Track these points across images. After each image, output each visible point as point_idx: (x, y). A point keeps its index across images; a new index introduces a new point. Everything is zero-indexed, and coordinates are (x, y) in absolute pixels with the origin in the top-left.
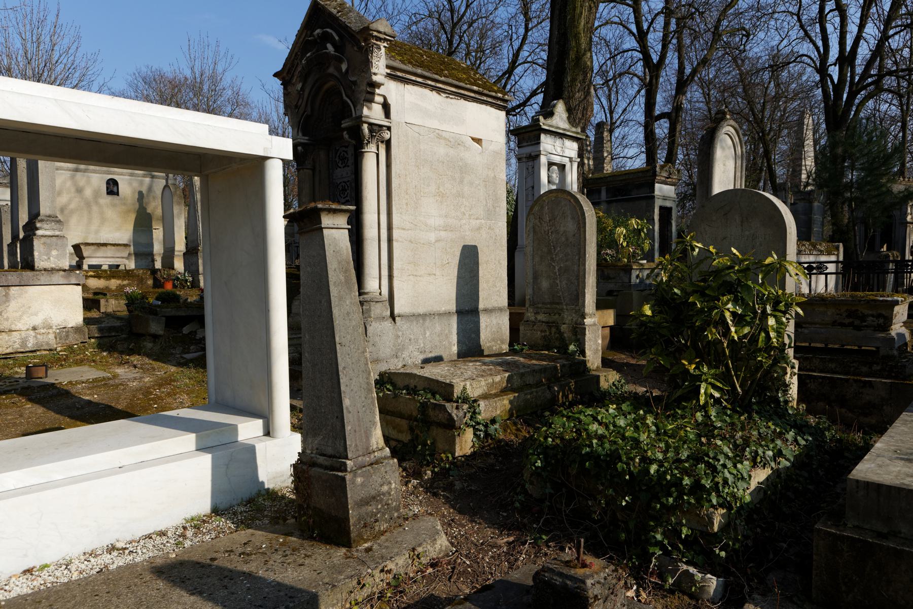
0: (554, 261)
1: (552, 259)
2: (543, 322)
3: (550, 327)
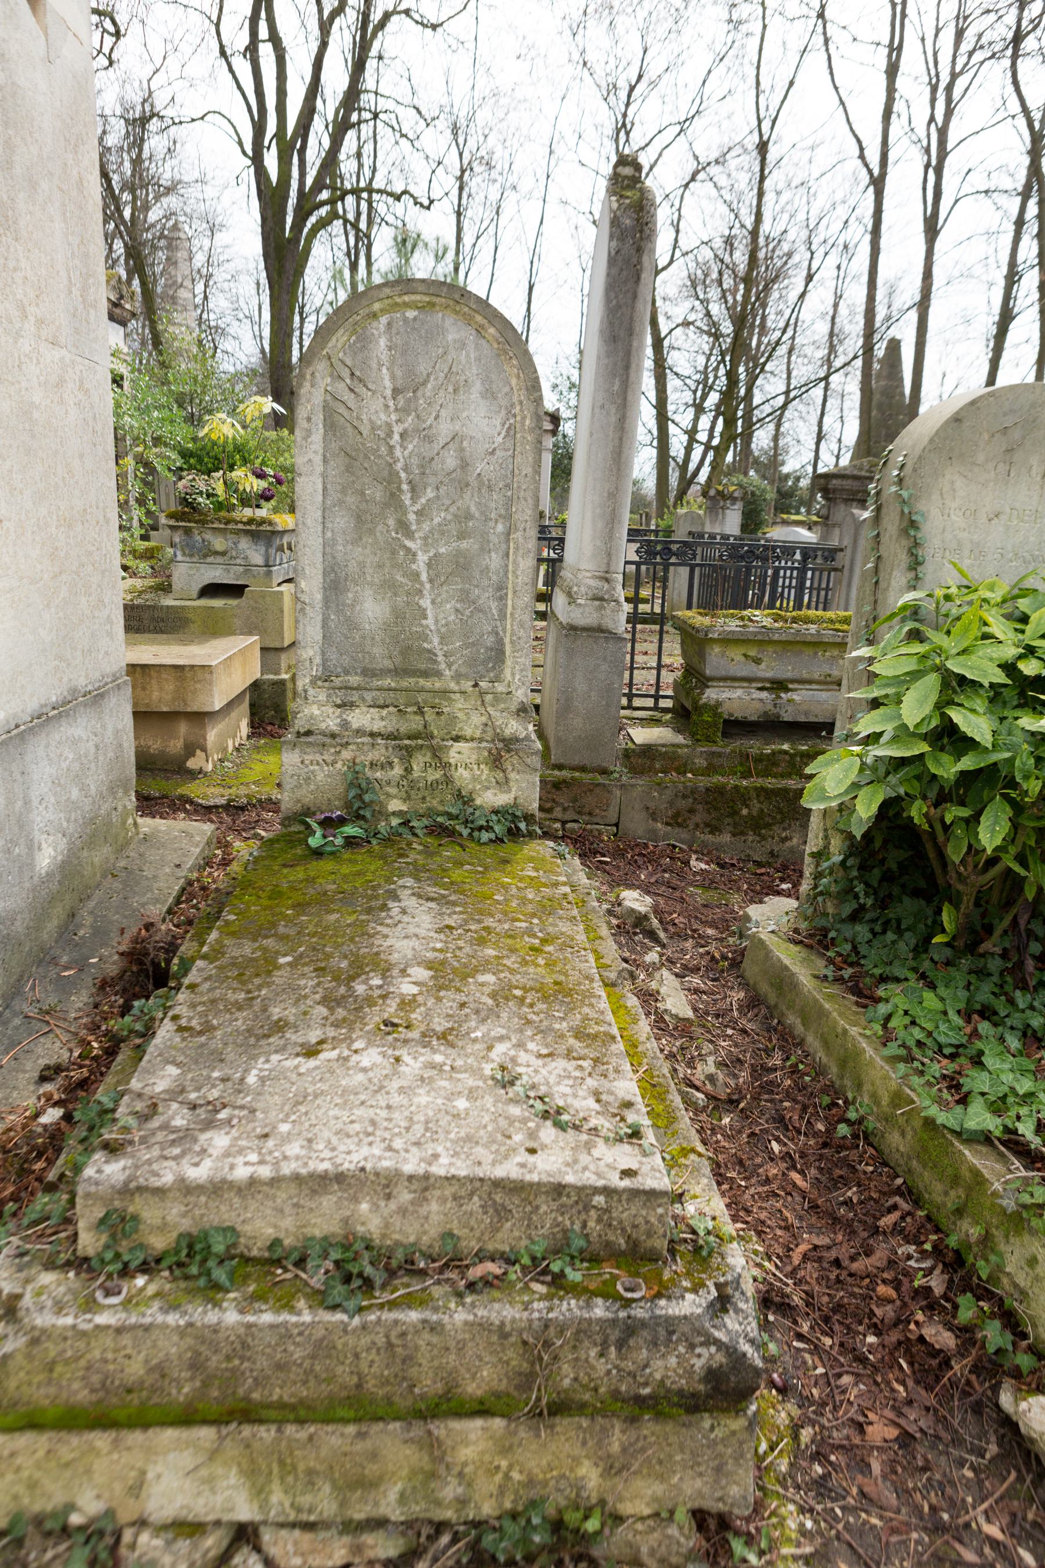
0: (410, 535)
1: (403, 526)
2: (372, 735)
3: (408, 753)
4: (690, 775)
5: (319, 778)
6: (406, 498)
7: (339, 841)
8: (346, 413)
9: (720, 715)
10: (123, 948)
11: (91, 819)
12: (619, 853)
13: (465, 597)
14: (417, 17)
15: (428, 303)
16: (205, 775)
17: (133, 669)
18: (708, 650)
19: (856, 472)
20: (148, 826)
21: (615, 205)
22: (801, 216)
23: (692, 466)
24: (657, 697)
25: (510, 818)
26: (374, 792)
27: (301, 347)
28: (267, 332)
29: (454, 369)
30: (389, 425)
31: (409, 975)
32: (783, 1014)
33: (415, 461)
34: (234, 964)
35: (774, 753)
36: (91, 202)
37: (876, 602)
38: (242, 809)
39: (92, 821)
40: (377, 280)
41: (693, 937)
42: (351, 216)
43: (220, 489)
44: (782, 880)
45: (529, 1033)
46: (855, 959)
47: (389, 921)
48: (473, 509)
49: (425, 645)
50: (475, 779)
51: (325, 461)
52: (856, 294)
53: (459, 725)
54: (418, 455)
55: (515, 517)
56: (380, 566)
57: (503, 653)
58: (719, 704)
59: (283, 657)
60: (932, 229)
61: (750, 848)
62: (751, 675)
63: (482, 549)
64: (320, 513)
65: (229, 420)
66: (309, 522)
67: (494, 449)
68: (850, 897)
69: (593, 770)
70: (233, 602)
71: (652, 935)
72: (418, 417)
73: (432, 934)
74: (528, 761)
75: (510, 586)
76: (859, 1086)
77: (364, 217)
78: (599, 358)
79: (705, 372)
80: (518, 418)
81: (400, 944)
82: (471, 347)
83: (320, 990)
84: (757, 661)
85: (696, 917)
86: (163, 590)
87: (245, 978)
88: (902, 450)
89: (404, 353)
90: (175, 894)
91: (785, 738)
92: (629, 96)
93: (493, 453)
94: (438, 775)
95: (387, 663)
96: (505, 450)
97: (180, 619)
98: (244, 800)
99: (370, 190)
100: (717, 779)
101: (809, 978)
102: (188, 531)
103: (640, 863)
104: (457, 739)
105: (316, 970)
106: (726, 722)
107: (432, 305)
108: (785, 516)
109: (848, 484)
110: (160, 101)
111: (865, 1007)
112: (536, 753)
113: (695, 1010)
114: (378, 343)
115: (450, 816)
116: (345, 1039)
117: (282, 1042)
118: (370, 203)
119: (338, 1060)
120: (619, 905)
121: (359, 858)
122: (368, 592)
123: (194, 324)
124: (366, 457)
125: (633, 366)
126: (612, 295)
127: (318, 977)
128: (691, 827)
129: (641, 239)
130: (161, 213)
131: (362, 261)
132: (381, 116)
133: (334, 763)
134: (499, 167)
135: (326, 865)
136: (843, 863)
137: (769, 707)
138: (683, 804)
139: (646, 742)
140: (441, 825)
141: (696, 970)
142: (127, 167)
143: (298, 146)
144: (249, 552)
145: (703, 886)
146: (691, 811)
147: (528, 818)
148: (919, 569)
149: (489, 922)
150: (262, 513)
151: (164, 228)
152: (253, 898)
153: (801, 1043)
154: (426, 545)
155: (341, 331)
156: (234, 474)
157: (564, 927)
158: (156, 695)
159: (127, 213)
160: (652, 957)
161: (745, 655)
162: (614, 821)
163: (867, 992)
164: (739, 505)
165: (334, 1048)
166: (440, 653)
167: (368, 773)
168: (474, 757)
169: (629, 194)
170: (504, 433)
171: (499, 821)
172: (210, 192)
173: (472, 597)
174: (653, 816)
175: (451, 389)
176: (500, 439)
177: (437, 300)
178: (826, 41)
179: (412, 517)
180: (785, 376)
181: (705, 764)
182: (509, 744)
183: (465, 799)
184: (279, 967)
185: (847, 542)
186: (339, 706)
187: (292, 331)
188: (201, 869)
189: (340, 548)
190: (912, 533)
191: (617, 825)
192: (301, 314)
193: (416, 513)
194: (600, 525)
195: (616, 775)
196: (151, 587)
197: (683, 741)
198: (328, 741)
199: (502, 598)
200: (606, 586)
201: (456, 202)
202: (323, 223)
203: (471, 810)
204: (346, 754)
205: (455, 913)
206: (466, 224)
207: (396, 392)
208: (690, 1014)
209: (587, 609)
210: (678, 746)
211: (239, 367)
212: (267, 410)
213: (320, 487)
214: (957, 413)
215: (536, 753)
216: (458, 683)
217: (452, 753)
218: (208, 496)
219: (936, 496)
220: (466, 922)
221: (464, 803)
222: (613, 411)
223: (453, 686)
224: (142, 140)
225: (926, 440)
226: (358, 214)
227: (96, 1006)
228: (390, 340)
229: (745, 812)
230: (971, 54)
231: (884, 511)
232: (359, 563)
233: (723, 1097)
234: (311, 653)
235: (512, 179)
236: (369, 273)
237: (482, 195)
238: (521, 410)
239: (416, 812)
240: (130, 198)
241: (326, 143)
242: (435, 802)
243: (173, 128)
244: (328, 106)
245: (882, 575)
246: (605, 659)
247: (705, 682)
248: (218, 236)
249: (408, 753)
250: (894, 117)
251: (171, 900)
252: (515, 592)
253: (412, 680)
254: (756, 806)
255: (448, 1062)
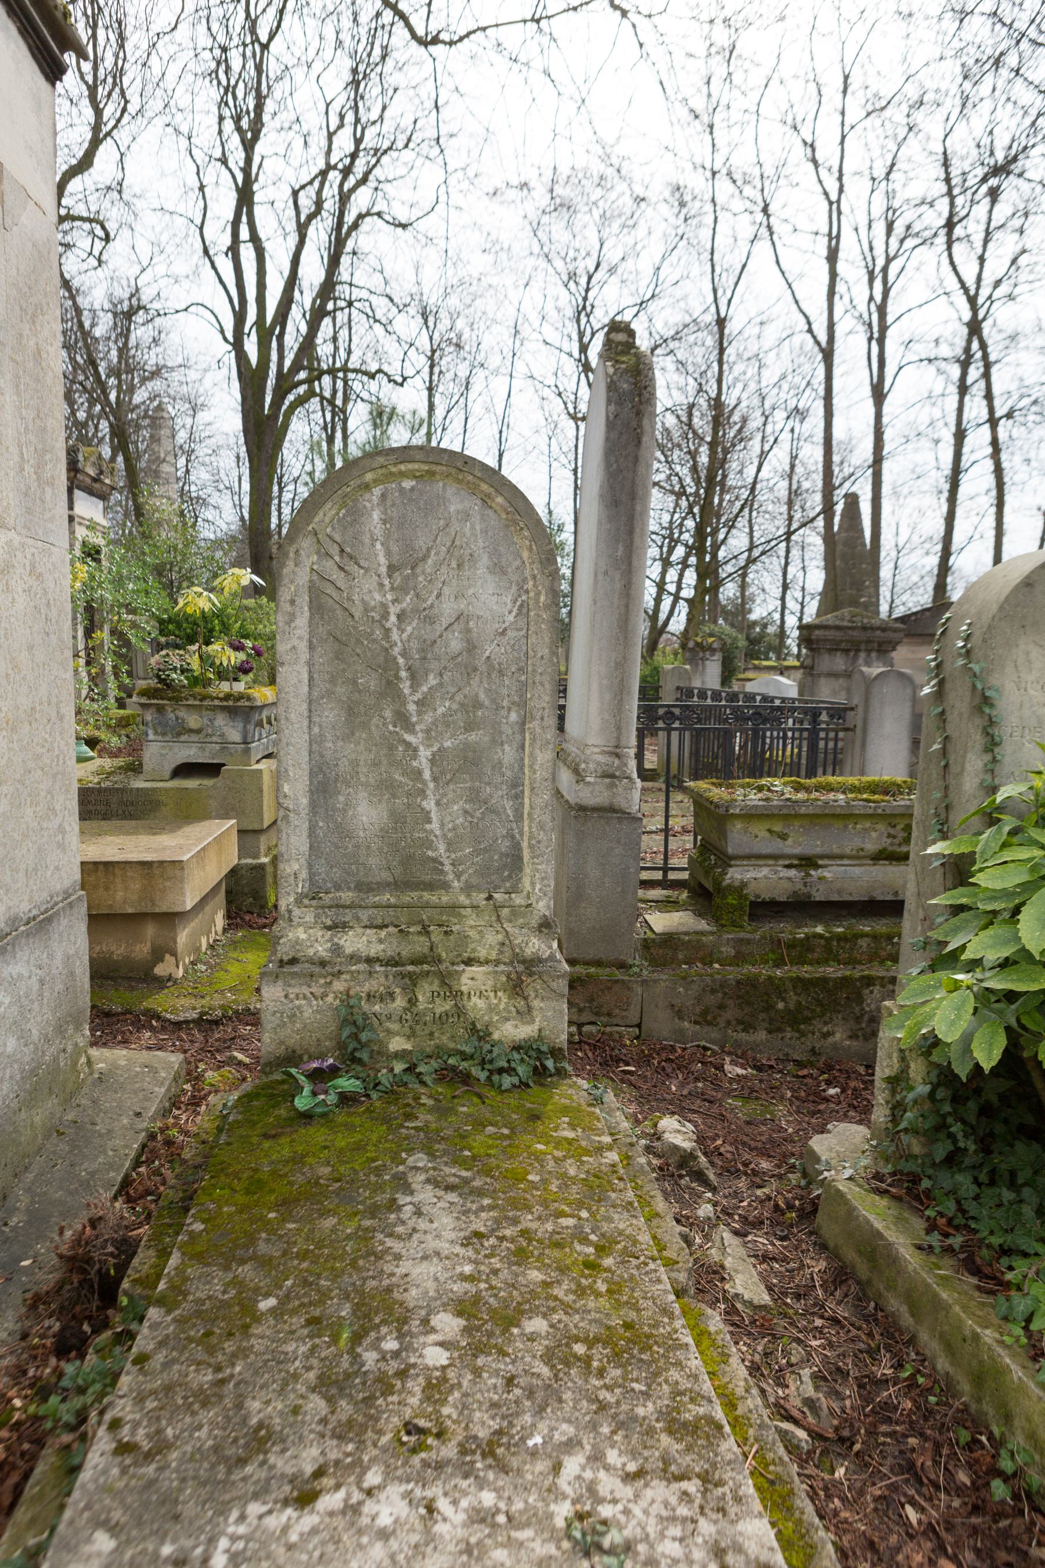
0: (410, 728)
1: (402, 719)
2: (369, 960)
4: (717, 966)
5: (306, 1015)
6: (405, 687)
7: (332, 1098)
8: (334, 594)
9: (744, 897)
10: (64, 1249)
11: (32, 1071)
12: (644, 1060)
13: (474, 796)
14: (387, 217)
15: (427, 471)
16: (175, 982)
17: (91, 869)
18: (729, 826)
19: (837, 623)
20: (105, 1061)
21: (611, 370)
22: (753, 386)
23: (662, 616)
24: (665, 869)
25: (534, 1054)
26: (372, 1029)
27: (280, 514)
28: (246, 501)
29: (457, 543)
30: (384, 606)
31: (433, 1330)
32: (880, 1295)
33: (414, 645)
34: (198, 1314)
35: (807, 938)
36: (50, 374)
37: (946, 788)
38: (217, 1023)
39: (33, 1072)
40: (354, 451)
41: (746, 1174)
42: (327, 394)
43: (195, 663)
44: (829, 1083)
45: (605, 1430)
46: (964, 1222)
47: (400, 1229)
48: (482, 696)
49: (430, 853)
50: (491, 1009)
51: (311, 647)
52: (812, 454)
53: (472, 946)
54: (418, 638)
55: (531, 704)
56: (376, 764)
57: (520, 858)
58: (744, 885)
59: (263, 839)
60: (879, 394)
61: (789, 1046)
62: (777, 852)
63: (494, 741)
64: (305, 706)
65: (205, 593)
66: (293, 717)
67: (505, 629)
68: (942, 1135)
69: (610, 964)
70: (208, 782)
71: (699, 1176)
72: (417, 596)
73: (458, 1249)
74: (554, 985)
75: (527, 782)
76: (1008, 1418)
77: (340, 395)
78: (600, 523)
79: (670, 528)
80: (532, 594)
81: (418, 1270)
82: (476, 518)
83: (315, 1362)
84: (783, 837)
85: (744, 1144)
86: (134, 770)
87: (214, 1340)
88: (964, 617)
89: (401, 526)
90: (133, 1154)
91: (818, 919)
92: (588, 283)
93: (503, 633)
94: (448, 1006)
95: (385, 876)
96: (518, 630)
97: (151, 802)
98: (219, 1013)
99: (345, 369)
100: (748, 969)
101: (912, 1249)
102: (160, 709)
103: (669, 1070)
104: (469, 962)
105: (309, 1322)
106: (753, 904)
107: (432, 473)
108: (756, 662)
109: (830, 634)
110: (146, 296)
111: (991, 1293)
112: (563, 976)
113: (770, 1289)
114: (371, 516)
115: (465, 1057)
116: (353, 1465)
117: (263, 1474)
118: (345, 381)
119: (343, 1512)
120: (659, 1139)
121: (357, 1121)
122: (362, 794)
123: (175, 496)
124: (358, 641)
125: (637, 530)
126: (613, 459)
127: (311, 1336)
128: (722, 1025)
129: (641, 402)
130: (146, 395)
131: (339, 435)
132: (356, 304)
133: (324, 996)
134: (467, 348)
135: (318, 1134)
136: (932, 1095)
137: (799, 886)
138: (712, 1000)
139: (667, 930)
140: (453, 1069)
141: (758, 1224)
142: (114, 353)
143: (277, 332)
144: (225, 729)
145: (741, 1097)
146: (722, 1007)
147: (555, 1053)
148: (996, 750)
149: (528, 1221)
150: (240, 687)
151: (146, 411)
152: (227, 1192)
153: (912, 1341)
154: (429, 738)
155: (329, 505)
156: (210, 648)
157: (621, 1222)
158: (120, 895)
159: (113, 396)
160: (705, 1210)
161: (769, 831)
162: (636, 1021)
163: (987, 1270)
164: (718, 656)
165: (338, 1487)
166: (447, 862)
167: (365, 1006)
168: (490, 983)
169: (624, 359)
170: (515, 610)
171: (522, 1060)
172: (193, 375)
173: (483, 796)
174: (680, 1014)
175: (454, 564)
176: (511, 618)
177: (438, 468)
178: (771, 234)
179: (412, 707)
180: (747, 530)
181: (733, 952)
182: (531, 965)
183: (480, 1033)
184: (257, 1318)
185: (856, 701)
186: (329, 928)
187: (271, 499)
188: (165, 1113)
189: (330, 745)
190: (987, 710)
191: (639, 1026)
192: (279, 484)
193: (417, 703)
194: (608, 697)
195: (636, 969)
196: (120, 768)
197: (707, 928)
198: (317, 970)
199: (518, 797)
200: (617, 762)
201: (427, 379)
202: (301, 401)
203: (488, 1047)
204: (339, 986)
205: (482, 1209)
206: (437, 399)
207: (392, 569)
208: (766, 1298)
209: (597, 788)
210: (702, 933)
211: (219, 534)
212: (245, 582)
213: (306, 676)
214: (1028, 577)
215: (563, 976)
216: (469, 896)
217: (464, 979)
218: (183, 671)
219: (1009, 669)
220: (497, 1221)
221: (480, 1039)
222: (618, 577)
223: (463, 899)
224: (128, 330)
225: (995, 608)
226: (334, 392)
227: (24, 1336)
228: (385, 512)
229: (781, 1005)
230: (902, 241)
231: (948, 686)
232: (351, 762)
233: (830, 1434)
234: (296, 867)
235: (480, 358)
236: (345, 445)
237: (452, 373)
238: (535, 586)
239: (422, 1051)
240: (116, 382)
241: (304, 329)
242: (445, 1039)
243: (158, 320)
244: (305, 298)
245: (952, 758)
246: (618, 842)
247: (726, 860)
248: (200, 415)
249: (412, 981)
250: (837, 297)
251: (127, 1164)
252: (532, 789)
253: (415, 894)
254: (793, 998)
255: (502, 1505)
